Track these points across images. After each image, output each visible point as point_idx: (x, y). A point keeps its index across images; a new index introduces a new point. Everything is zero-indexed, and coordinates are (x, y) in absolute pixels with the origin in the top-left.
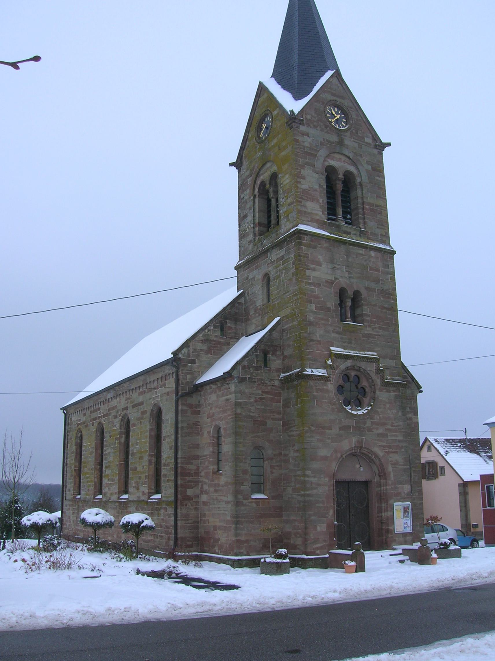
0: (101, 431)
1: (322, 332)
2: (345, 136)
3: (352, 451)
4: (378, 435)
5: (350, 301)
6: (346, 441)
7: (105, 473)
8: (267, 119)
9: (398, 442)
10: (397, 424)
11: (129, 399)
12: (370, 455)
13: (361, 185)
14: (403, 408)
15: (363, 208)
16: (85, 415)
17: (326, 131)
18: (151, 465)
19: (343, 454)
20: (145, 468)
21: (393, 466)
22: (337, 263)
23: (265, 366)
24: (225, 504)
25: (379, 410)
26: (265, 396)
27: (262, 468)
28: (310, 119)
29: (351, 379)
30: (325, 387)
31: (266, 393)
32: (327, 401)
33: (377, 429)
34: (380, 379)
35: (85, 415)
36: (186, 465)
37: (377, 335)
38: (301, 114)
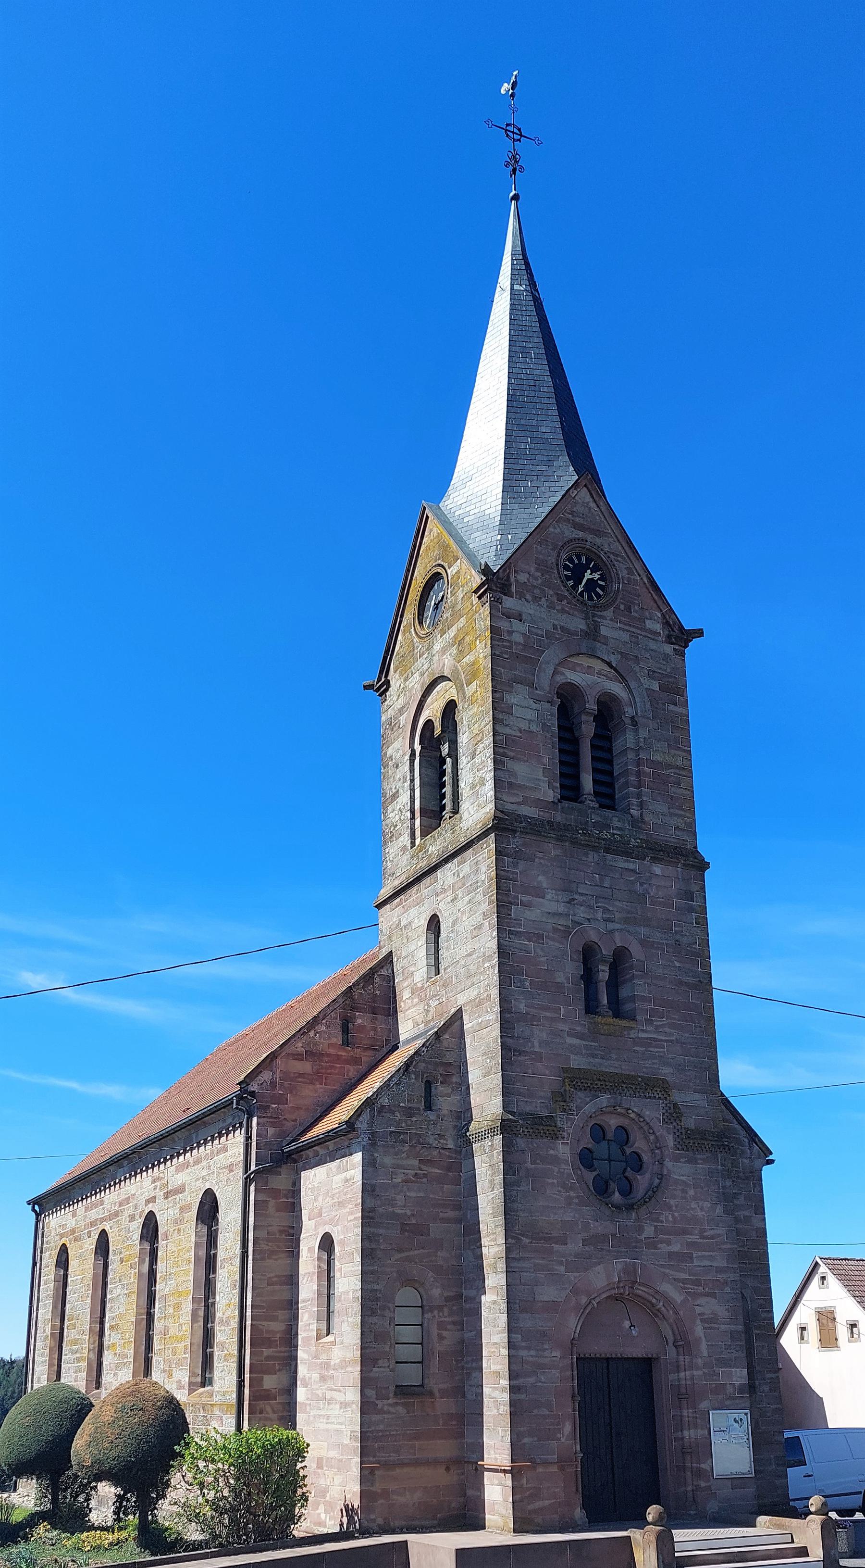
0: (103, 1246)
1: (544, 1035)
2: (601, 617)
3: (613, 1292)
4: (670, 1255)
5: (607, 968)
6: (600, 1268)
7: (109, 1341)
8: (439, 585)
9: (716, 1271)
10: (711, 1233)
11: (159, 1179)
12: (654, 1301)
13: (634, 723)
14: (726, 1199)
15: (639, 774)
16: (74, 1215)
17: (559, 607)
18: (198, 1321)
19: (593, 1296)
20: (184, 1329)
21: (706, 1325)
22: (580, 891)
23: (429, 1107)
24: (341, 1408)
25: (672, 1202)
26: (427, 1169)
27: (420, 1327)
28: (525, 583)
29: (610, 1135)
30: (551, 1152)
31: (430, 1162)
32: (555, 1181)
33: (669, 1243)
34: (672, 1133)
35: (74, 1215)
36: (264, 1323)
37: (666, 1041)
38: (505, 571)
